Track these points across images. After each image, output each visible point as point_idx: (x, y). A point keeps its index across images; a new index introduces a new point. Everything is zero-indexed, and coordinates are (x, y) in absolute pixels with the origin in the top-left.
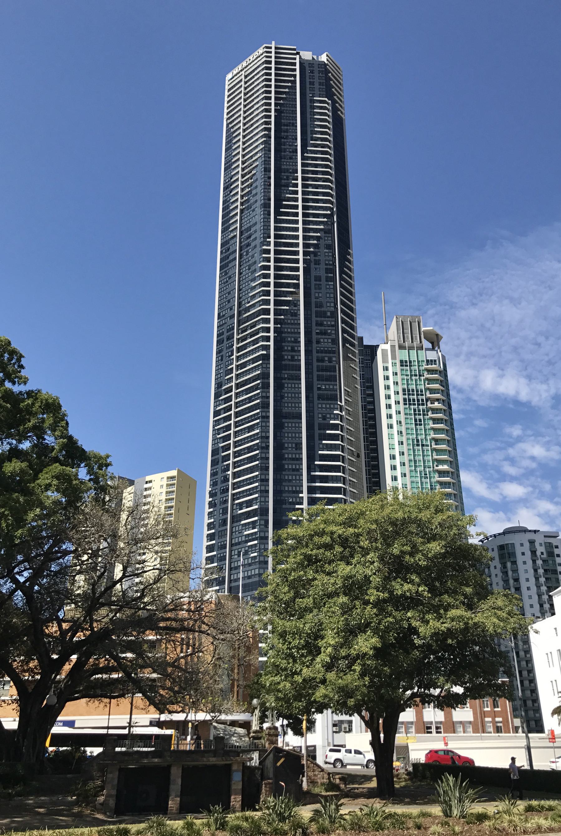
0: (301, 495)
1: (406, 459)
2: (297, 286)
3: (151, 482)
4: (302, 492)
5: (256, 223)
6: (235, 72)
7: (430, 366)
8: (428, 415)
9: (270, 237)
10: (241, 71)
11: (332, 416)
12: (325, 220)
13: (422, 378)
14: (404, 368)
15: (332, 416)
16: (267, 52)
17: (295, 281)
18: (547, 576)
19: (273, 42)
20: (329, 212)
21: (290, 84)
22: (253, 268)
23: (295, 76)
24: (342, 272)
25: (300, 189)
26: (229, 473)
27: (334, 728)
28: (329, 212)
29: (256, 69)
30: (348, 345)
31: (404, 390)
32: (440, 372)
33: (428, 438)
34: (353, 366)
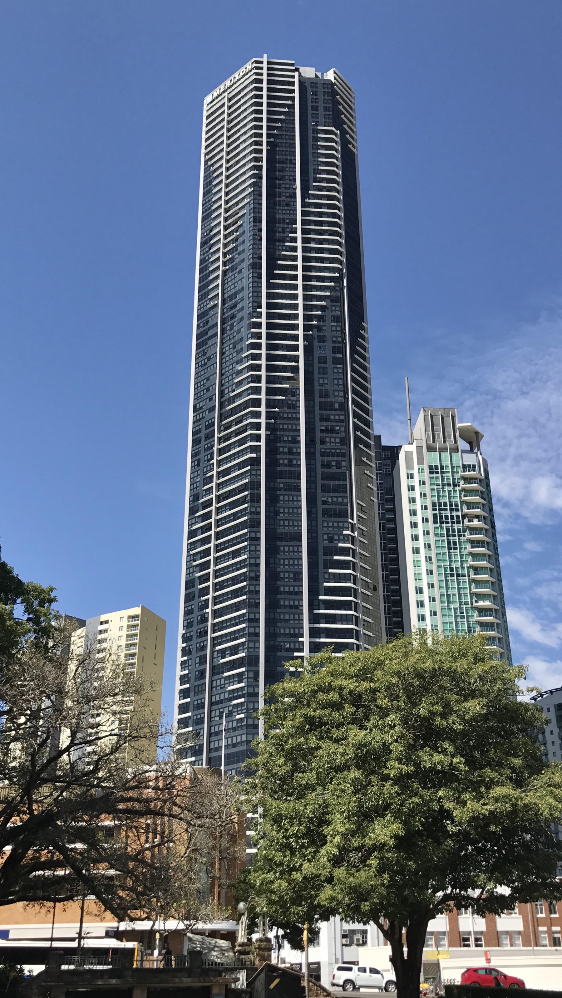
1: (436, 592)
2: (296, 370)
5: (242, 289)
6: (215, 94)
7: (467, 473)
8: (464, 536)
9: (260, 307)
10: (224, 92)
12: (332, 284)
13: (457, 488)
14: (440, 538)
15: (341, 537)
16: (257, 68)
17: (293, 364)
19: (265, 56)
20: (337, 275)
21: (286, 110)
23: (293, 99)
24: (354, 351)
25: (299, 244)
28: (337, 275)
29: (243, 90)
31: (434, 504)
32: (480, 480)
33: (466, 565)
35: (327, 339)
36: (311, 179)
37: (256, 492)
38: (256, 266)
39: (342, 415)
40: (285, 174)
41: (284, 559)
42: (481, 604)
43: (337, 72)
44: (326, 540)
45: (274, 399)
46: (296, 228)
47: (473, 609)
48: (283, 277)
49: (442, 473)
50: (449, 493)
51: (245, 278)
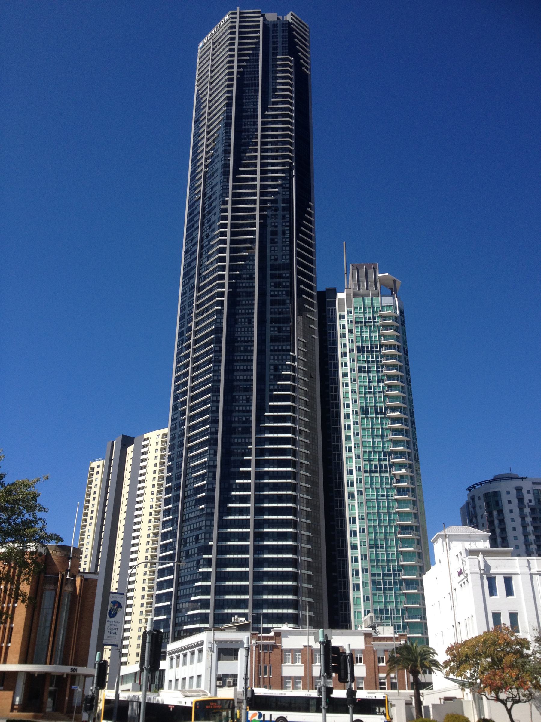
0: (250, 447)
2: (253, 241)
3: (148, 439)
4: (250, 444)
5: (216, 184)
6: (205, 41)
8: (381, 361)
9: (228, 197)
11: (284, 367)
12: (283, 175)
13: (377, 325)
16: (232, 18)
18: (536, 525)
19: (238, 8)
20: (287, 167)
21: (253, 46)
22: (212, 227)
23: (258, 38)
25: (259, 147)
26: (185, 427)
27: (218, 682)
28: (287, 167)
30: (304, 296)
33: (393, 524)
34: (310, 316)
35: (278, 26)
36: (267, 398)
37: (219, 335)
38: (226, 173)
39: (287, 273)
40: (249, 134)
41: (241, 337)
42: (391, 393)
43: (294, 14)
44: (272, 369)
45: (236, 265)
46: (257, 135)
47: (393, 488)
48: (246, 180)
49: (369, 372)
50: (385, 530)
51: (218, 178)
